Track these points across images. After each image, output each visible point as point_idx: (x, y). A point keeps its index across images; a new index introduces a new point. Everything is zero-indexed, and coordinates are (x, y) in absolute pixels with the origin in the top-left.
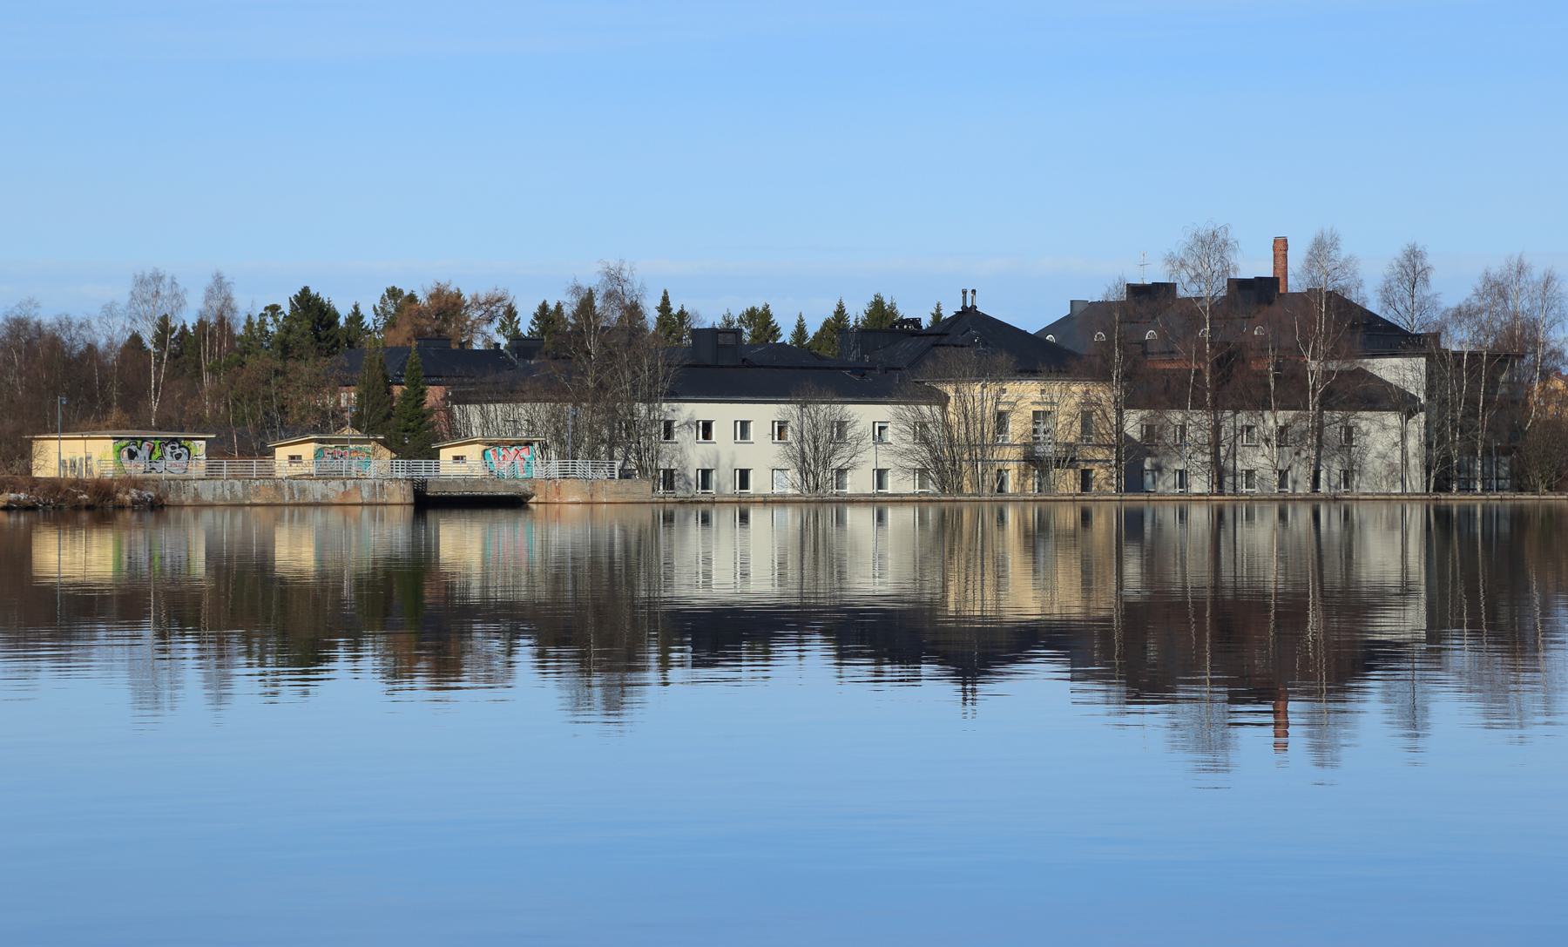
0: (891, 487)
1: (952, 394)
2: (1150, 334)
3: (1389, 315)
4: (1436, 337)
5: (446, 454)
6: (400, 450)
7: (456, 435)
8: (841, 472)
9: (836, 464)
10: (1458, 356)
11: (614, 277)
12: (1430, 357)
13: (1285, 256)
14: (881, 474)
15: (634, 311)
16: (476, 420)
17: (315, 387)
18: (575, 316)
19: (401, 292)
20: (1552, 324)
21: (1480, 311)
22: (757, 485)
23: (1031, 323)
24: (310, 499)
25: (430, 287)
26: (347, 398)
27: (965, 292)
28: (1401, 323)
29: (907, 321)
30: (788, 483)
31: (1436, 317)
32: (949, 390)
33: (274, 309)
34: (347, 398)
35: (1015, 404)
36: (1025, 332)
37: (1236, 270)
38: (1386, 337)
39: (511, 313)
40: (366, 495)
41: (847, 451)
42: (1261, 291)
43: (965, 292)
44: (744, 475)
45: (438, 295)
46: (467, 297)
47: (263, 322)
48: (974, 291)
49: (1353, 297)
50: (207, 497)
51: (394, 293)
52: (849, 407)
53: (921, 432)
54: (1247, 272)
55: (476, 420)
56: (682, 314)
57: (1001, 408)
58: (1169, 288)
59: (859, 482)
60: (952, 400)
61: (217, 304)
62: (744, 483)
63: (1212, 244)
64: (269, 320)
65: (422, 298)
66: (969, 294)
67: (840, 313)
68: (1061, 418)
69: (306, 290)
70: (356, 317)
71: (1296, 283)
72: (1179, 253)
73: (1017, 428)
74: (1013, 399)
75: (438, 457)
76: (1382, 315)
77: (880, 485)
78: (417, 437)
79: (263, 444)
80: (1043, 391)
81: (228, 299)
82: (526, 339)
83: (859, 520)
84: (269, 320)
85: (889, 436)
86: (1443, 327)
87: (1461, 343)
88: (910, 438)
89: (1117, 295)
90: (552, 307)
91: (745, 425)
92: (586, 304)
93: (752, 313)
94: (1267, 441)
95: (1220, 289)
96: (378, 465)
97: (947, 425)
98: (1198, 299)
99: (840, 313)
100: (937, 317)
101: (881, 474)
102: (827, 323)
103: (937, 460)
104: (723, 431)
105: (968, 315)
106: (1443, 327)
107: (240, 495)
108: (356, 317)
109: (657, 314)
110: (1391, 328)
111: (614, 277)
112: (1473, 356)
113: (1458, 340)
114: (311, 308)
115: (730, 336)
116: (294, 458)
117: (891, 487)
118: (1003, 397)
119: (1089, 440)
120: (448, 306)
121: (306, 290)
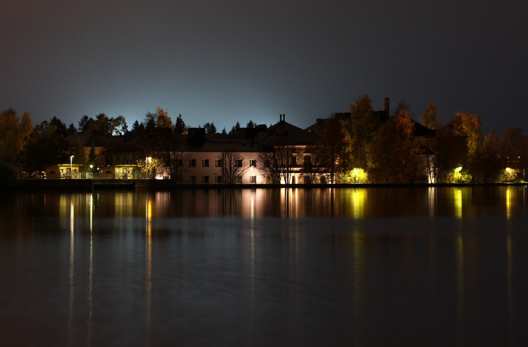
36: (196, 128)
43: (281, 115)
64: (44, 124)
70: (72, 126)
108: (72, 126)
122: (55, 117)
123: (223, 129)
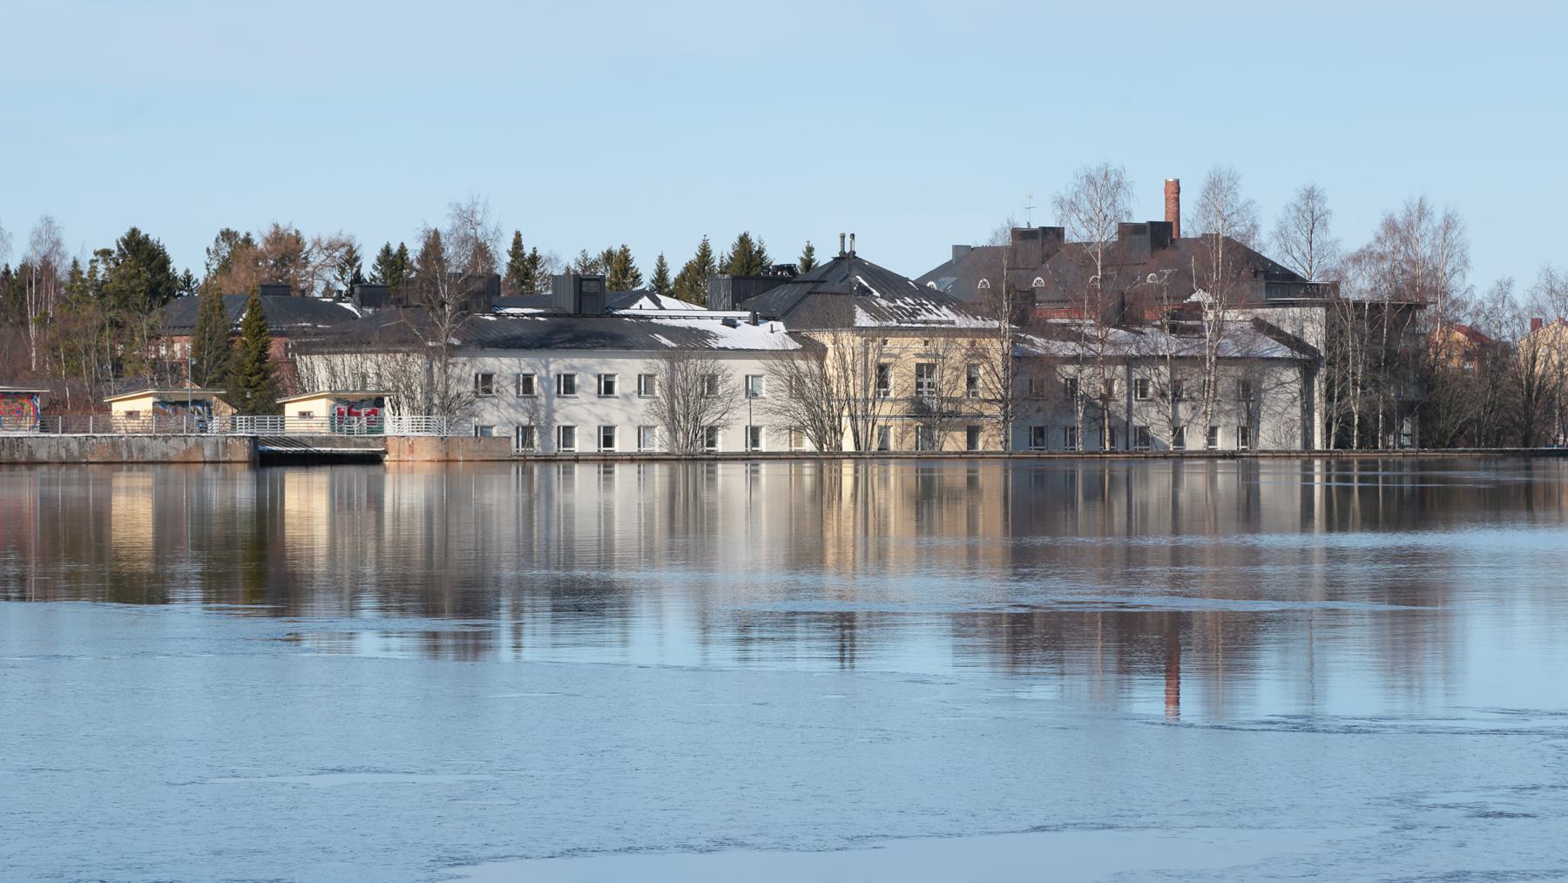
0: (764, 446)
1: (830, 346)
2: (1038, 281)
3: (1287, 263)
4: (1335, 286)
5: (292, 410)
6: (244, 407)
7: (300, 388)
8: (712, 431)
9: (707, 421)
10: (1358, 305)
11: (467, 217)
12: (1328, 306)
13: (1177, 200)
14: (754, 433)
15: (481, 252)
16: (322, 374)
17: (154, 337)
18: (419, 261)
19: (235, 234)
20: (1454, 271)
21: (1382, 257)
22: (624, 442)
23: (911, 268)
24: (150, 457)
25: (267, 230)
26: (181, 348)
27: (843, 237)
28: (1300, 272)
29: (781, 268)
30: (658, 442)
31: (1332, 263)
32: (826, 338)
33: (106, 253)
34: (181, 348)
35: (897, 357)
37: (1129, 214)
38: (1282, 284)
39: (352, 259)
40: (208, 453)
41: (720, 407)
42: (1161, 234)
43: (843, 237)
44: (568, 431)
45: (277, 238)
46: (308, 238)
47: (93, 270)
48: (853, 236)
49: (1253, 245)
50: (42, 455)
51: (227, 235)
52: (722, 361)
53: (796, 386)
54: (1141, 218)
55: (322, 374)
56: (534, 259)
57: (882, 360)
58: (1058, 233)
59: (730, 440)
60: (830, 353)
61: (43, 249)
62: (608, 441)
63: (1106, 185)
65: (258, 241)
66: (848, 239)
67: (705, 253)
68: (947, 373)
69: (134, 232)
71: (1190, 227)
72: (1068, 195)
73: (900, 381)
74: (896, 351)
75: (282, 412)
76: (1279, 263)
77: (755, 442)
78: (261, 389)
79: (100, 397)
80: (926, 343)
81: (58, 243)
82: (370, 286)
83: (731, 478)
84: (101, 268)
85: (764, 388)
86: (1340, 274)
87: (1360, 292)
88: (785, 395)
89: (1004, 240)
90: (395, 249)
91: (528, 380)
92: (433, 246)
93: (609, 257)
94: (1163, 395)
95: (1111, 234)
96: (226, 425)
97: (824, 378)
98: (1088, 244)
99: (705, 253)
100: (808, 263)
101: (754, 433)
102: (688, 268)
103: (814, 418)
104: (587, 383)
105: (847, 261)
106: (1340, 274)
107: (76, 453)
109: (508, 259)
110: (1291, 276)
111: (467, 217)
112: (1376, 307)
113: (1359, 286)
114: (141, 253)
115: (593, 284)
116: (132, 409)
117: (764, 446)
118: (885, 350)
119: (974, 394)
120: (287, 248)
121: (134, 232)
122: (744, 241)
123: (383, 246)
